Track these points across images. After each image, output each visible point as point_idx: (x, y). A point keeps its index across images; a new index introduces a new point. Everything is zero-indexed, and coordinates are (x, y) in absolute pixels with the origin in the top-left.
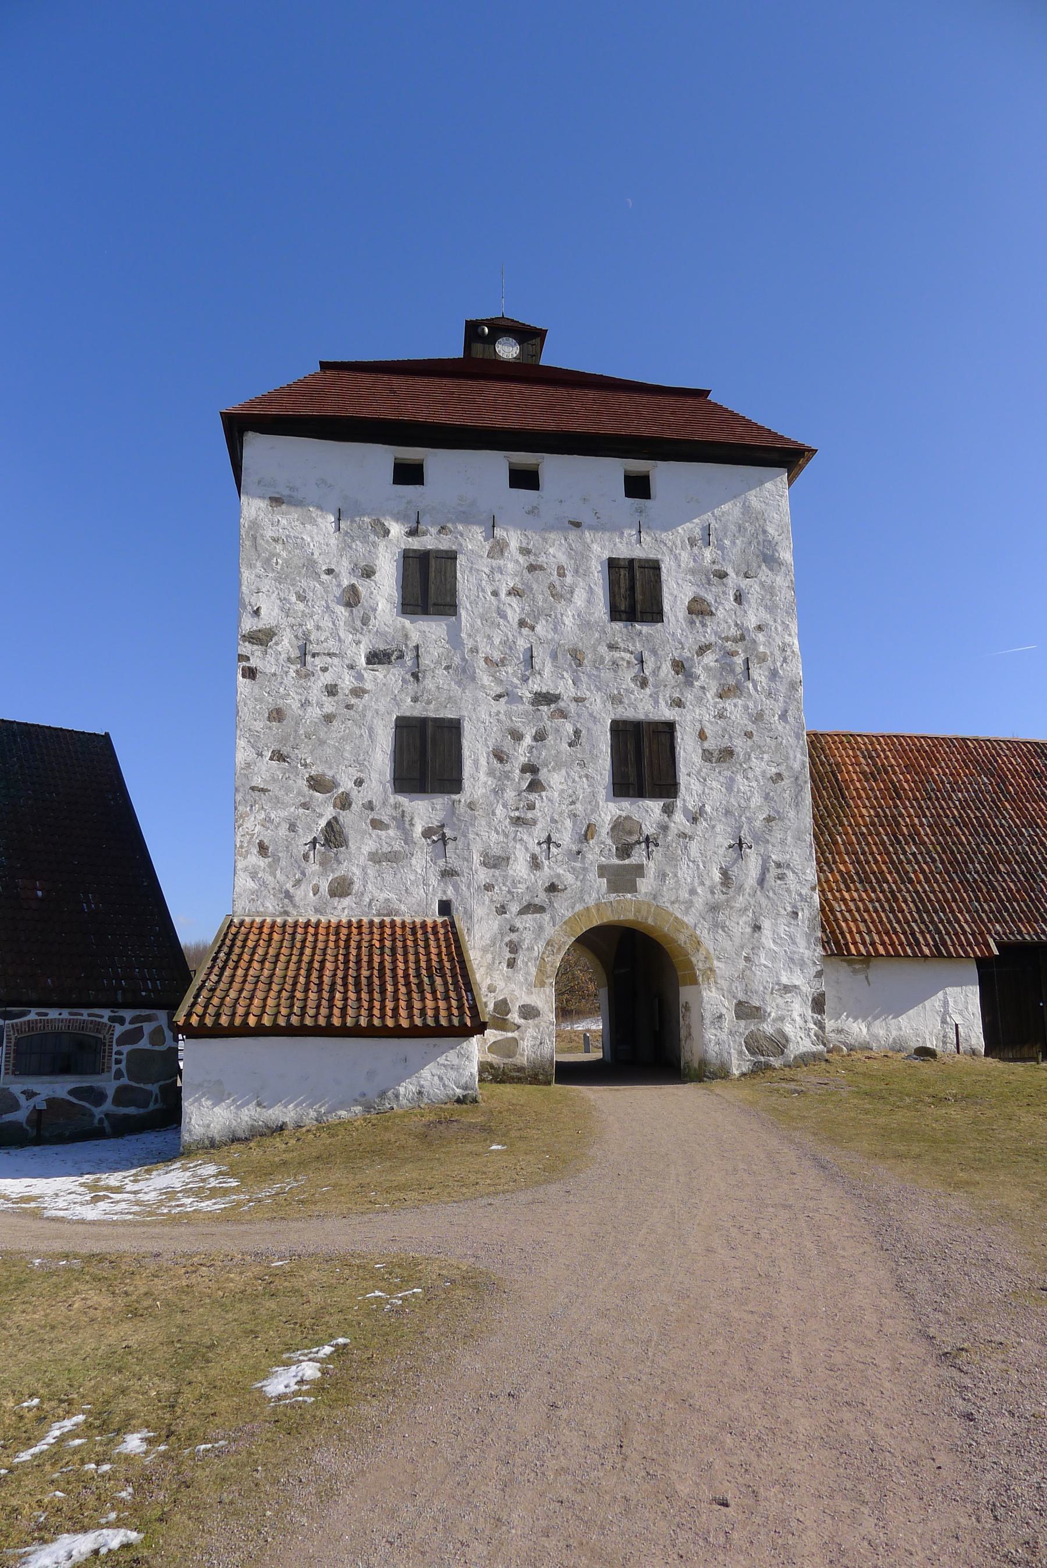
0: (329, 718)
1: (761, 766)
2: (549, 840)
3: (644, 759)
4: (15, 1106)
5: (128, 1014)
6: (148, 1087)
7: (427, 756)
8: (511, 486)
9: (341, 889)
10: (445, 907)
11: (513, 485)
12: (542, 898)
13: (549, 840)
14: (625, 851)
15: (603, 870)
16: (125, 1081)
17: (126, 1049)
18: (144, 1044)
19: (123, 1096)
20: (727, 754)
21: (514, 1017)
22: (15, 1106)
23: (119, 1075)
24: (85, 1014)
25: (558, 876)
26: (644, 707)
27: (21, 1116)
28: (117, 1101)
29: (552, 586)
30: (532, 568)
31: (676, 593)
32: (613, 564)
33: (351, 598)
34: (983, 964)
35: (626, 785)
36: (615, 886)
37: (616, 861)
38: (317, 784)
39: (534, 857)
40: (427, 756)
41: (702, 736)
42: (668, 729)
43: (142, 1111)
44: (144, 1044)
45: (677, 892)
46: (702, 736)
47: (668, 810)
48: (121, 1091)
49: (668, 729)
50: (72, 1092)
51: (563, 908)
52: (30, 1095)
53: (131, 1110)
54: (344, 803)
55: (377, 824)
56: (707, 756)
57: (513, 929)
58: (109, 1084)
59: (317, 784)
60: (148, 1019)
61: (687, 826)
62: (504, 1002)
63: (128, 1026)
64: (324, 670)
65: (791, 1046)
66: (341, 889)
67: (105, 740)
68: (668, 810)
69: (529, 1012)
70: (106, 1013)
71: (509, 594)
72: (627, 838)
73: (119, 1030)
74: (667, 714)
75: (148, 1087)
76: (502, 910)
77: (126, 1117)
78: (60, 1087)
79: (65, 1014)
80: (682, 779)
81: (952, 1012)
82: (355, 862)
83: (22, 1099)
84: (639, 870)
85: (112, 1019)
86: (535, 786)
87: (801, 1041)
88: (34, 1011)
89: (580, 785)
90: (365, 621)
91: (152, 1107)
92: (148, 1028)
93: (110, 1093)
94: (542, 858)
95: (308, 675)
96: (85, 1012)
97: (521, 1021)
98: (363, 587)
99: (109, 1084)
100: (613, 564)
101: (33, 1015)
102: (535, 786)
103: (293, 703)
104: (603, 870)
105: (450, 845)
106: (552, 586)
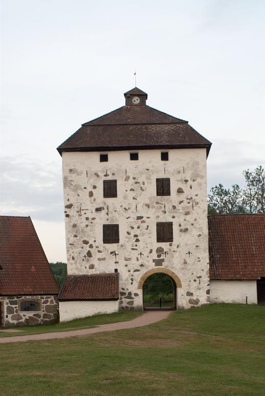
0: (87, 226)
1: (195, 233)
2: (141, 254)
3: (165, 232)
4: (22, 318)
5: (45, 297)
6: (51, 314)
7: (111, 234)
8: (116, 197)
9: (92, 267)
10: (116, 270)
11: (131, 159)
12: (139, 268)
13: (141, 254)
14: (159, 256)
15: (154, 261)
16: (45, 312)
17: (45, 305)
18: (49, 304)
19: (45, 316)
20: (186, 230)
21: (133, 296)
22: (22, 318)
23: (44, 311)
24: (35, 297)
25: (144, 262)
26: (166, 218)
27: (23, 320)
28: (43, 317)
29: (141, 188)
30: (136, 183)
31: (173, 188)
32: (157, 180)
33: (91, 194)
34: (258, 281)
35: (160, 239)
36: (156, 265)
37: (158, 258)
38: (86, 242)
39: (137, 258)
40: (111, 234)
41: (180, 225)
42: (171, 224)
43: (49, 320)
44: (49, 304)
45: (174, 265)
46: (180, 225)
47: (171, 245)
48: (44, 315)
49: (171, 224)
50: (33, 315)
51: (144, 271)
52: (24, 316)
53: (47, 319)
54: (91, 246)
55: (99, 251)
56: (181, 231)
57: (132, 276)
58: (42, 313)
59: (86, 242)
60: (49, 298)
61: (176, 249)
62: (130, 292)
63: (45, 300)
64: (85, 214)
65: (200, 302)
66: (92, 267)
67: (26, 222)
68: (171, 245)
69: (136, 295)
70: (40, 297)
71: (131, 190)
72: (160, 251)
73: (43, 300)
74: (170, 220)
75: (51, 314)
76: (129, 271)
77: (46, 321)
78: (29, 314)
79: (30, 297)
80: (174, 236)
81: (244, 293)
82: (94, 261)
83: (23, 316)
84: (163, 260)
85: (41, 298)
86: (137, 240)
87: (203, 300)
88: (24, 296)
89: (150, 239)
90: (95, 200)
91: (52, 319)
92: (49, 300)
93: (42, 315)
94: (139, 258)
95: (81, 215)
96: (35, 296)
97: (134, 297)
98: (94, 191)
99: (42, 313)
100: (157, 180)
101: (23, 298)
102: (137, 240)
103: (78, 223)
104: (154, 261)
105: (117, 255)
106: (141, 188)
